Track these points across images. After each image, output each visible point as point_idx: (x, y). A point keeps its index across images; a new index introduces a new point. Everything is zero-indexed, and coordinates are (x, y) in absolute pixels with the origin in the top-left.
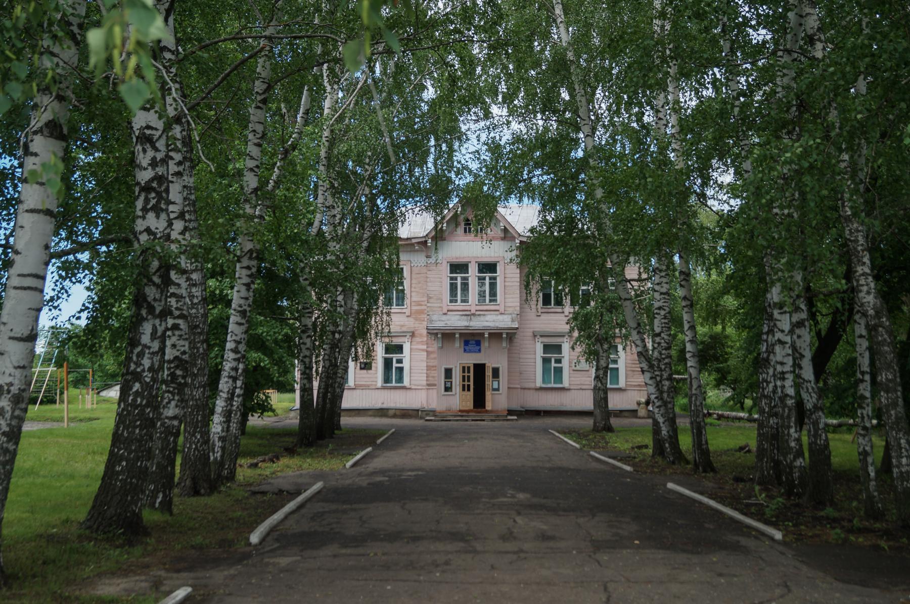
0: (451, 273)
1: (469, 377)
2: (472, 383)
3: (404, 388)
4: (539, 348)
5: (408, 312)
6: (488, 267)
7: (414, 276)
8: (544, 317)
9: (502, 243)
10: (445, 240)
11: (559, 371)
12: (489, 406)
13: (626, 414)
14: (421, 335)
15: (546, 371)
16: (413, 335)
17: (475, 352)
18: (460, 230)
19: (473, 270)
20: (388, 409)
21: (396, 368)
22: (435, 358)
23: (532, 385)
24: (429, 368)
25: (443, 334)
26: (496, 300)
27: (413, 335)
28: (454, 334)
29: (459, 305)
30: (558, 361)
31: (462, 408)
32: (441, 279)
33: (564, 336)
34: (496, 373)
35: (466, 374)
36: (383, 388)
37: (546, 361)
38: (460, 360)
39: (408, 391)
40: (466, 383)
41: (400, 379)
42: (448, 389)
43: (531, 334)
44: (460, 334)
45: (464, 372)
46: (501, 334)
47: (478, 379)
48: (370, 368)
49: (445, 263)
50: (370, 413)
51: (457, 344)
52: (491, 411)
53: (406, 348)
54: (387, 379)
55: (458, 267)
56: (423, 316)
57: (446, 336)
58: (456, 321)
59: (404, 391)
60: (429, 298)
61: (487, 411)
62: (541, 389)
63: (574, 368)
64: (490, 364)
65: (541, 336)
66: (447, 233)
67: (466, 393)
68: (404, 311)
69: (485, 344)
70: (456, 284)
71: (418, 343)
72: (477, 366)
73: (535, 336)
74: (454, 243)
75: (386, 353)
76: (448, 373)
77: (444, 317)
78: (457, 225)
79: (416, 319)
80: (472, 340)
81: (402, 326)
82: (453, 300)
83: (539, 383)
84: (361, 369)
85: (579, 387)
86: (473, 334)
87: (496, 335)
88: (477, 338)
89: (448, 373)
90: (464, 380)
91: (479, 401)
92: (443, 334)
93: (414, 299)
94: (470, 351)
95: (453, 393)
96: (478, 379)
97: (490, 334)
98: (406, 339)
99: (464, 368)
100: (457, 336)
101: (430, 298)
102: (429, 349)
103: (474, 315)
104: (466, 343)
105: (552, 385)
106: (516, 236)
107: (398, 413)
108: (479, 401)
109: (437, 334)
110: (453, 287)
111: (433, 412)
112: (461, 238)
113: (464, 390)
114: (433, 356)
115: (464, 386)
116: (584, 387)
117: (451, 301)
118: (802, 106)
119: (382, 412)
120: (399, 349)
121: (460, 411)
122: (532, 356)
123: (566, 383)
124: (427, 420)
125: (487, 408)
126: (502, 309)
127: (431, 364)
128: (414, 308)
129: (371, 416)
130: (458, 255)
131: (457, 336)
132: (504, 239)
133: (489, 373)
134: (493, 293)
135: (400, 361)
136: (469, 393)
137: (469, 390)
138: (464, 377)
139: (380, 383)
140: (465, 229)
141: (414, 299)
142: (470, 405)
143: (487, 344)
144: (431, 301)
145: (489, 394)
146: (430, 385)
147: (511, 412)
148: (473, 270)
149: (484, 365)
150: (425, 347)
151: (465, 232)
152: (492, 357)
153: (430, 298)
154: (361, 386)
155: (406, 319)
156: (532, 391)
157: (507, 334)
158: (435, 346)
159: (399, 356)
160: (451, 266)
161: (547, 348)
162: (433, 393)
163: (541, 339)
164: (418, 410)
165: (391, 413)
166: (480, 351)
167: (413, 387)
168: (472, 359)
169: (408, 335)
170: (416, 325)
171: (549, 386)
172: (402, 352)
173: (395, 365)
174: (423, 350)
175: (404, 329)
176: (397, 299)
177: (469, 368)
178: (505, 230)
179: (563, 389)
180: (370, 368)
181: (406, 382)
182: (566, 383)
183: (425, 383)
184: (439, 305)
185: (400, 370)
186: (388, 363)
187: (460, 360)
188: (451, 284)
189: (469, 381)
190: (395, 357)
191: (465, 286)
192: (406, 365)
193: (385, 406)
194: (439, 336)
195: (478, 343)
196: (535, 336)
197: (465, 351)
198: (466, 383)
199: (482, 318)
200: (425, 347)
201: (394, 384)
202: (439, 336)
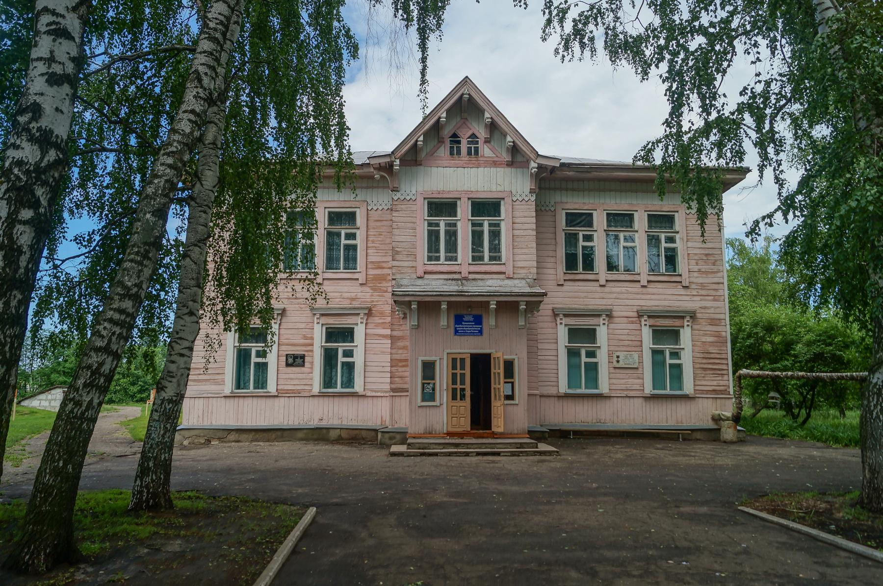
0: (430, 215)
1: (463, 376)
2: (468, 386)
3: (355, 395)
4: (562, 333)
5: (362, 278)
6: (486, 207)
7: (371, 224)
8: (569, 286)
9: (508, 170)
10: (421, 165)
11: (592, 369)
12: (498, 425)
13: (698, 435)
14: (382, 314)
15: (573, 368)
16: (369, 313)
17: (472, 334)
18: (444, 151)
19: (464, 210)
20: (328, 429)
21: (343, 363)
22: (405, 348)
23: (552, 391)
24: (394, 363)
25: (419, 303)
26: (499, 259)
27: (369, 313)
28: (439, 303)
29: (443, 265)
30: (591, 354)
31: (451, 430)
32: (415, 226)
33: (599, 316)
34: (509, 367)
35: (458, 371)
36: (322, 395)
37: (573, 353)
38: (448, 347)
39: (361, 400)
40: (458, 386)
41: (349, 382)
42: (429, 396)
43: (550, 313)
44: (450, 304)
45: (454, 367)
46: (517, 303)
47: (479, 381)
48: (303, 365)
49: (420, 200)
50: (300, 435)
51: (443, 322)
52: (501, 435)
53: (360, 332)
54: (328, 382)
55: (442, 207)
56: (384, 284)
57: (426, 307)
58: (436, 285)
59: (355, 399)
60: (395, 253)
61: (494, 435)
62: (567, 396)
63: (615, 364)
64: (500, 354)
65: (565, 316)
66: (423, 154)
67: (458, 403)
68: (356, 276)
69: (490, 322)
70: (438, 232)
71: (378, 325)
72: (475, 358)
73: (556, 315)
74: (434, 169)
75: (327, 342)
76: (429, 369)
77: (420, 282)
78: (441, 141)
79: (374, 289)
80: (468, 313)
81: (353, 299)
82: (433, 255)
83: (563, 388)
84: (288, 365)
85: (624, 394)
86: (469, 305)
87: (509, 306)
88: (476, 312)
89: (429, 369)
90: (454, 382)
91: (481, 417)
92: (419, 303)
93: (371, 259)
94: (465, 334)
95: (437, 403)
96: (479, 381)
97: (498, 303)
98: (358, 320)
99: (454, 360)
100: (444, 306)
101: (398, 253)
102: (395, 333)
103: (466, 279)
104: (459, 319)
105: (583, 390)
106: (532, 156)
107: (344, 434)
108: (481, 417)
109: (409, 303)
110: (433, 236)
111: (402, 437)
112: (445, 163)
113: (454, 398)
114: (400, 344)
115: (454, 391)
116: (632, 394)
117: (430, 259)
118: (724, 133)
119: (318, 435)
120: (347, 334)
121: (450, 434)
122: (553, 346)
123: (604, 387)
124: (394, 454)
125: (494, 429)
126: (509, 270)
127: (398, 357)
128: (371, 272)
129: (301, 439)
130: (441, 187)
131: (444, 306)
132: (511, 164)
133: (497, 370)
134: (495, 248)
135: (348, 354)
136: (462, 403)
137: (463, 397)
138: (454, 376)
139: (316, 388)
140: (452, 148)
141: (371, 259)
142: (465, 423)
143: (492, 322)
144: (398, 257)
145: (498, 406)
146: (397, 391)
147: (537, 436)
148: (464, 210)
149: (488, 356)
150: (388, 332)
151: (452, 154)
152: (499, 343)
153: (398, 253)
154: (287, 391)
155: (360, 289)
156: (552, 399)
157: (528, 303)
158: (405, 328)
159: (347, 345)
160: (430, 204)
161: (574, 334)
162: (403, 404)
163: (566, 321)
164: (376, 431)
165: (333, 434)
166: (481, 332)
167: (369, 394)
168: (468, 346)
169: (362, 312)
170: (376, 299)
171: (579, 391)
172: (352, 341)
173: (341, 359)
174: (384, 336)
175: (356, 304)
176: (347, 259)
177: (463, 360)
178: (515, 150)
179: (600, 396)
180: (303, 365)
181: (358, 386)
182: (604, 387)
183: (388, 387)
184: (410, 264)
185: (349, 367)
186: (330, 357)
187: (448, 347)
188: (430, 233)
189: (463, 382)
190: (341, 347)
191: (452, 235)
192: (358, 359)
193: (324, 424)
194: (414, 306)
195: (478, 320)
196: (556, 315)
197: (456, 332)
198: (458, 386)
199: (480, 283)
200: (388, 332)
201: (339, 389)
202: (414, 306)
